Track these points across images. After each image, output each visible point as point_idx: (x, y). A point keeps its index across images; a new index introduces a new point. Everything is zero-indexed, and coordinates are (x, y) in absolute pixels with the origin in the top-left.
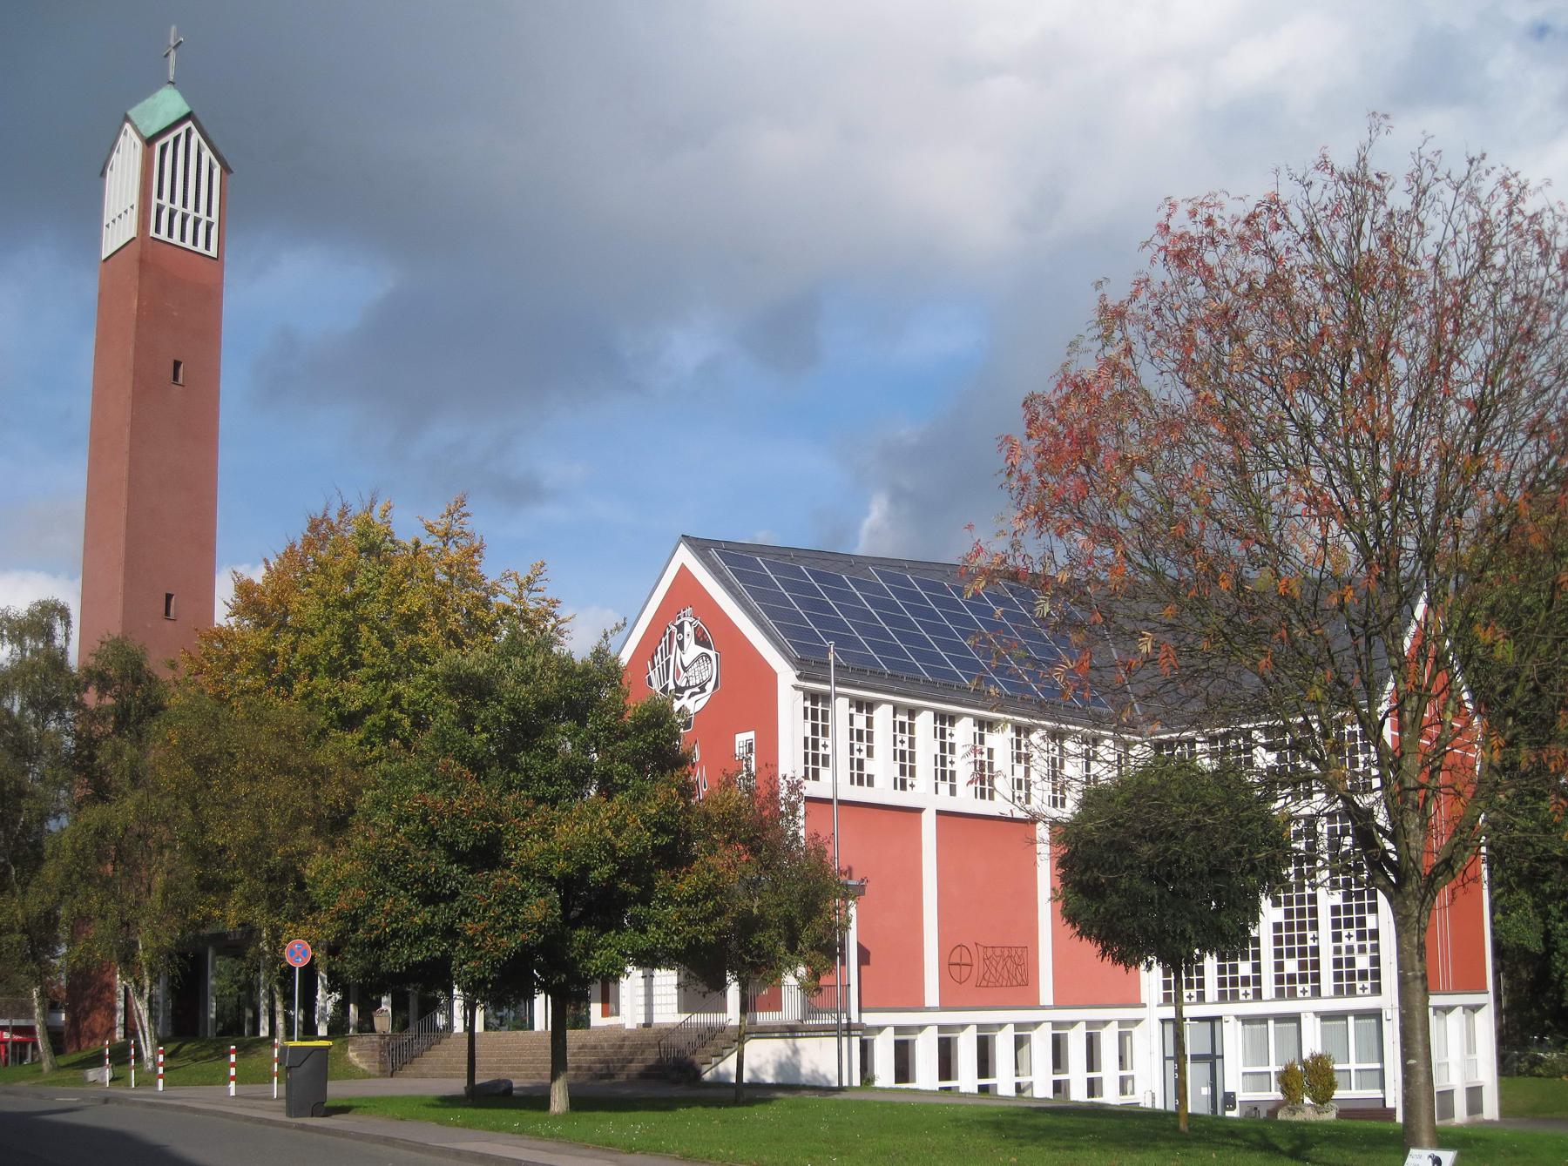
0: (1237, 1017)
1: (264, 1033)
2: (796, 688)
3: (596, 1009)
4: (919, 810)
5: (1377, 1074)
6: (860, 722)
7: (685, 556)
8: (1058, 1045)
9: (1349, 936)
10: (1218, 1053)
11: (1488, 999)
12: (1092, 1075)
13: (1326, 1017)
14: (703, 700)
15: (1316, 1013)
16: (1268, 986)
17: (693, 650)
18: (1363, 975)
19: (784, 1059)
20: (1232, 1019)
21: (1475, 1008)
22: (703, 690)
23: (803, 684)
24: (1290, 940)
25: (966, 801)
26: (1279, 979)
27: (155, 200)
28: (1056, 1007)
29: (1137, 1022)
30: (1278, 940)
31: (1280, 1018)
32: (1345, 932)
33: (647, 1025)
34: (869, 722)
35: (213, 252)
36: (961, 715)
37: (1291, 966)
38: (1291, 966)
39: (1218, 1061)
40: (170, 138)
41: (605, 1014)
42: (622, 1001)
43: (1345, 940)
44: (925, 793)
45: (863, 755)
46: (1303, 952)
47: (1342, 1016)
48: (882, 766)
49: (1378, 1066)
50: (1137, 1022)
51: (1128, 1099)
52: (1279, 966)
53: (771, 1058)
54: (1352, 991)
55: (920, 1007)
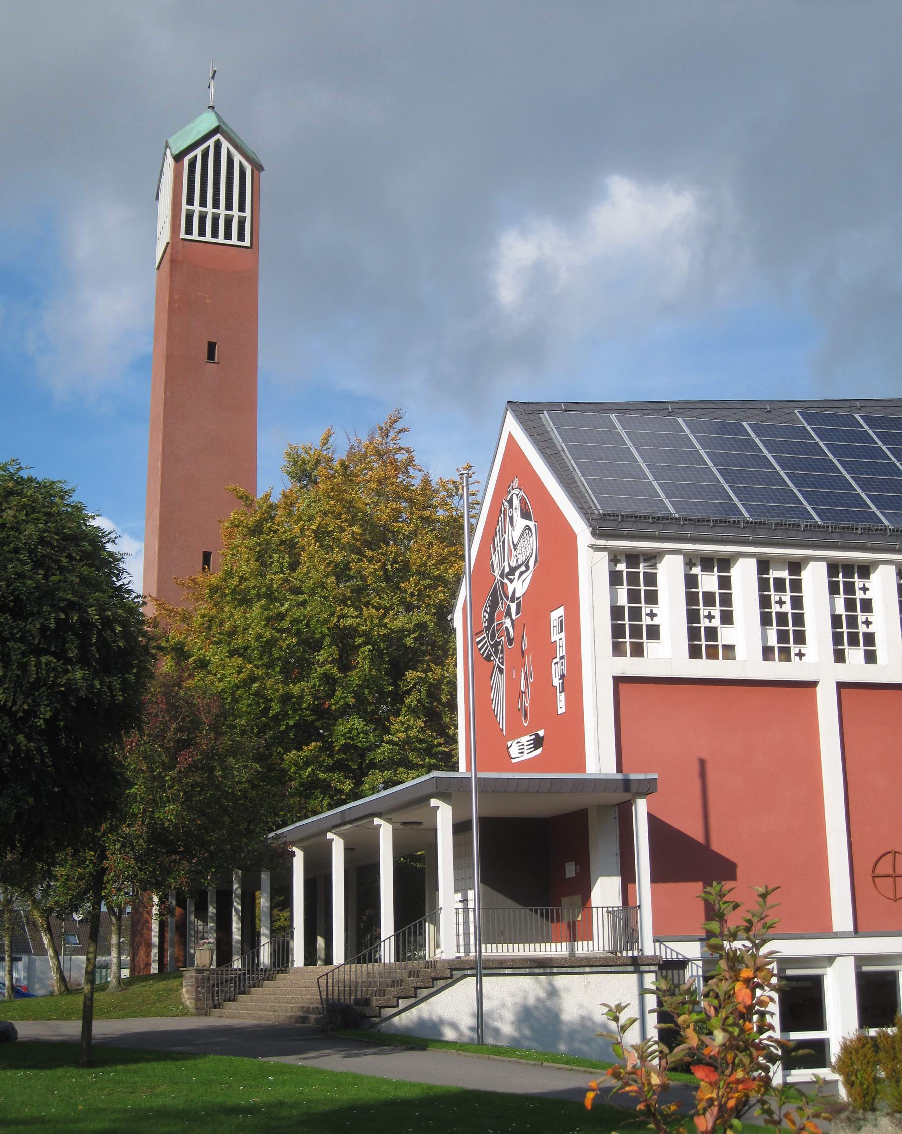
1: (265, 955)
2: (596, 548)
4: (813, 684)
6: (708, 582)
7: (512, 426)
14: (528, 576)
17: (520, 523)
19: (531, 1001)
22: (527, 568)
23: (602, 543)
27: (185, 207)
28: (857, 932)
34: (725, 583)
35: (247, 243)
36: (808, 560)
40: (199, 152)
44: (815, 661)
45: (716, 622)
48: (744, 633)
53: (509, 1000)
55: (825, 931)
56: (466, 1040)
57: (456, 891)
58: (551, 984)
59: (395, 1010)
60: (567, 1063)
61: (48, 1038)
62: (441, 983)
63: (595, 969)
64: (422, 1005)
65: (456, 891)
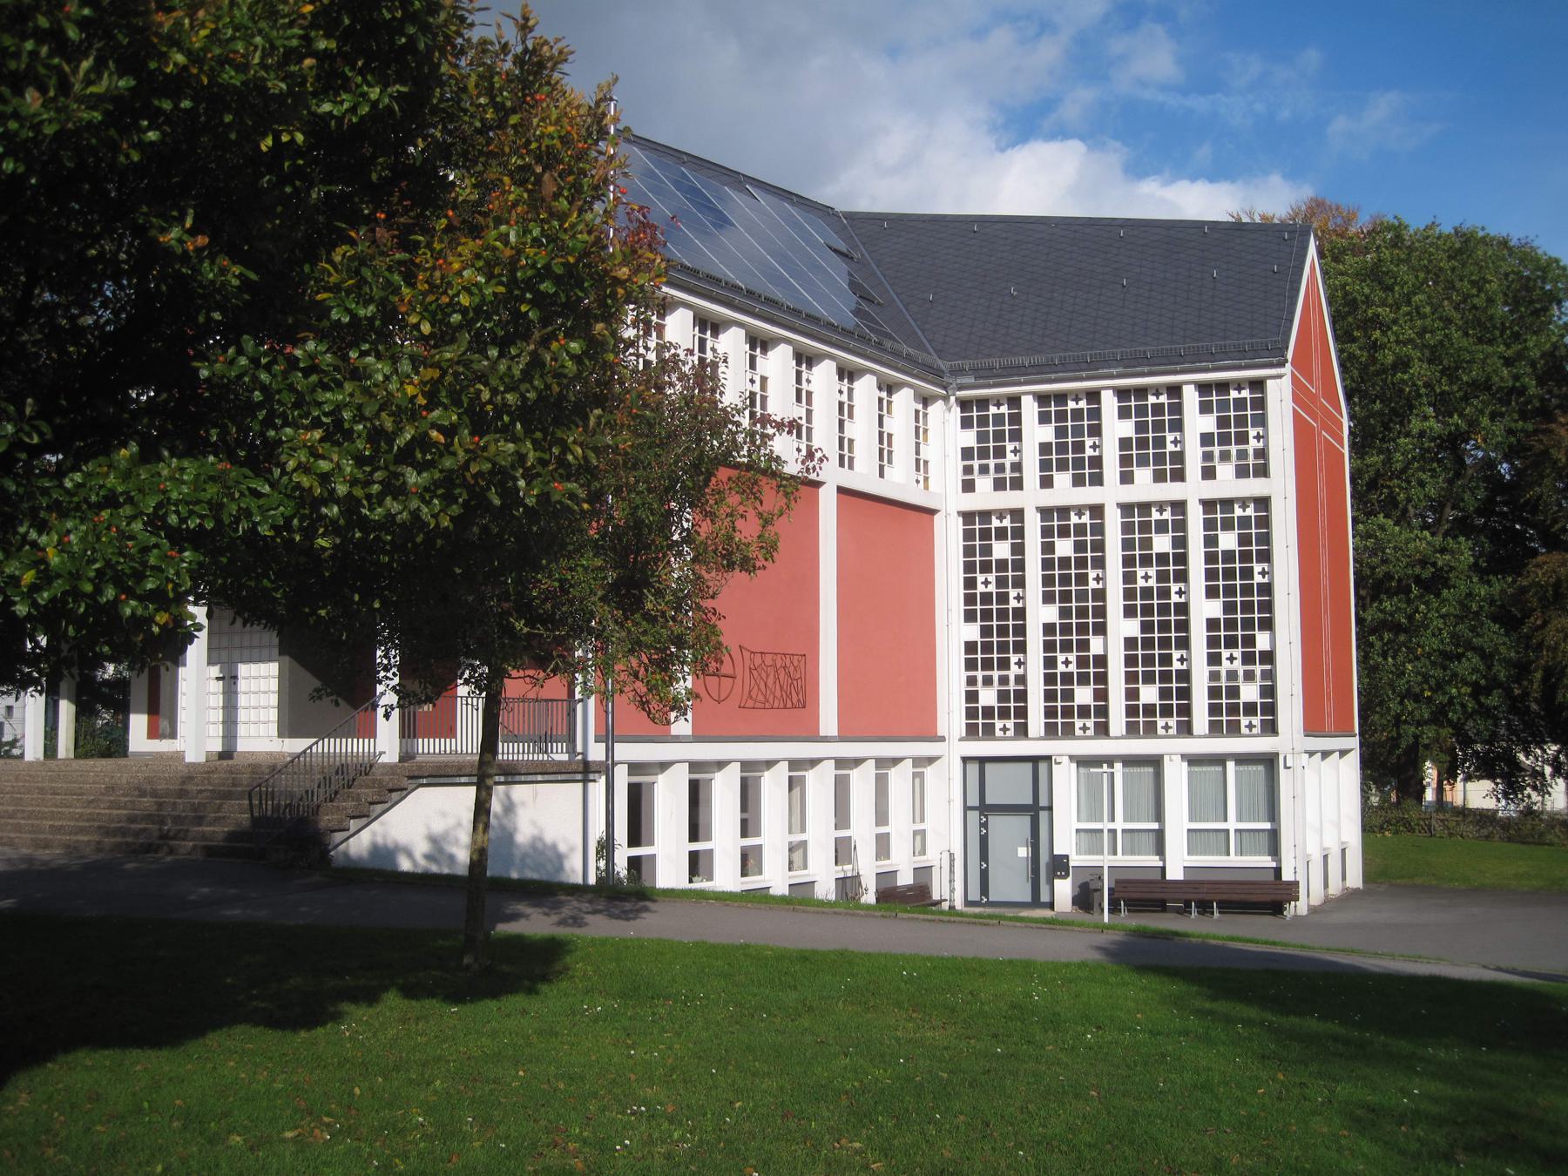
0: (1071, 758)
3: (138, 723)
5: (1152, 836)
8: (697, 796)
9: (1231, 659)
10: (1043, 802)
11: (1354, 743)
12: (696, 846)
13: (1193, 760)
15: (1184, 757)
16: (1117, 718)
18: (1250, 709)
20: (1065, 760)
21: (1343, 753)
24: (1148, 660)
25: (863, 477)
26: (1132, 711)
28: (842, 738)
29: (931, 760)
30: (1130, 661)
31: (1130, 761)
32: (1225, 653)
33: (227, 754)
37: (1149, 694)
38: (1149, 694)
39: (1043, 815)
41: (153, 733)
42: (182, 716)
43: (1226, 664)
46: (1165, 677)
47: (1219, 760)
49: (1155, 826)
50: (931, 760)
51: (753, 882)
52: (1132, 694)
54: (1234, 729)
56: (419, 871)
57: (210, 663)
58: (508, 797)
59: (346, 834)
60: (1001, 918)
61: (1317, 955)
62: (395, 796)
63: (547, 777)
64: (375, 825)
65: (210, 663)
